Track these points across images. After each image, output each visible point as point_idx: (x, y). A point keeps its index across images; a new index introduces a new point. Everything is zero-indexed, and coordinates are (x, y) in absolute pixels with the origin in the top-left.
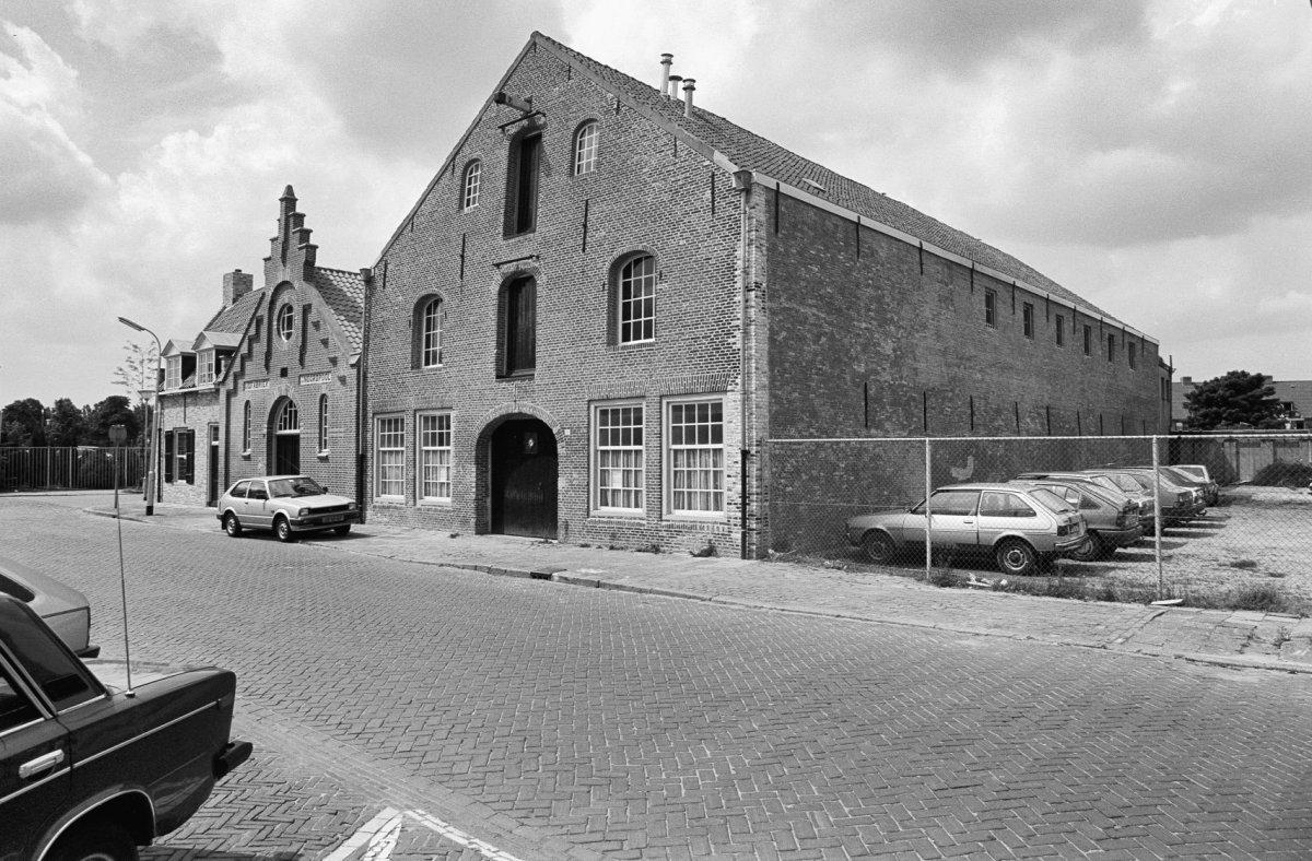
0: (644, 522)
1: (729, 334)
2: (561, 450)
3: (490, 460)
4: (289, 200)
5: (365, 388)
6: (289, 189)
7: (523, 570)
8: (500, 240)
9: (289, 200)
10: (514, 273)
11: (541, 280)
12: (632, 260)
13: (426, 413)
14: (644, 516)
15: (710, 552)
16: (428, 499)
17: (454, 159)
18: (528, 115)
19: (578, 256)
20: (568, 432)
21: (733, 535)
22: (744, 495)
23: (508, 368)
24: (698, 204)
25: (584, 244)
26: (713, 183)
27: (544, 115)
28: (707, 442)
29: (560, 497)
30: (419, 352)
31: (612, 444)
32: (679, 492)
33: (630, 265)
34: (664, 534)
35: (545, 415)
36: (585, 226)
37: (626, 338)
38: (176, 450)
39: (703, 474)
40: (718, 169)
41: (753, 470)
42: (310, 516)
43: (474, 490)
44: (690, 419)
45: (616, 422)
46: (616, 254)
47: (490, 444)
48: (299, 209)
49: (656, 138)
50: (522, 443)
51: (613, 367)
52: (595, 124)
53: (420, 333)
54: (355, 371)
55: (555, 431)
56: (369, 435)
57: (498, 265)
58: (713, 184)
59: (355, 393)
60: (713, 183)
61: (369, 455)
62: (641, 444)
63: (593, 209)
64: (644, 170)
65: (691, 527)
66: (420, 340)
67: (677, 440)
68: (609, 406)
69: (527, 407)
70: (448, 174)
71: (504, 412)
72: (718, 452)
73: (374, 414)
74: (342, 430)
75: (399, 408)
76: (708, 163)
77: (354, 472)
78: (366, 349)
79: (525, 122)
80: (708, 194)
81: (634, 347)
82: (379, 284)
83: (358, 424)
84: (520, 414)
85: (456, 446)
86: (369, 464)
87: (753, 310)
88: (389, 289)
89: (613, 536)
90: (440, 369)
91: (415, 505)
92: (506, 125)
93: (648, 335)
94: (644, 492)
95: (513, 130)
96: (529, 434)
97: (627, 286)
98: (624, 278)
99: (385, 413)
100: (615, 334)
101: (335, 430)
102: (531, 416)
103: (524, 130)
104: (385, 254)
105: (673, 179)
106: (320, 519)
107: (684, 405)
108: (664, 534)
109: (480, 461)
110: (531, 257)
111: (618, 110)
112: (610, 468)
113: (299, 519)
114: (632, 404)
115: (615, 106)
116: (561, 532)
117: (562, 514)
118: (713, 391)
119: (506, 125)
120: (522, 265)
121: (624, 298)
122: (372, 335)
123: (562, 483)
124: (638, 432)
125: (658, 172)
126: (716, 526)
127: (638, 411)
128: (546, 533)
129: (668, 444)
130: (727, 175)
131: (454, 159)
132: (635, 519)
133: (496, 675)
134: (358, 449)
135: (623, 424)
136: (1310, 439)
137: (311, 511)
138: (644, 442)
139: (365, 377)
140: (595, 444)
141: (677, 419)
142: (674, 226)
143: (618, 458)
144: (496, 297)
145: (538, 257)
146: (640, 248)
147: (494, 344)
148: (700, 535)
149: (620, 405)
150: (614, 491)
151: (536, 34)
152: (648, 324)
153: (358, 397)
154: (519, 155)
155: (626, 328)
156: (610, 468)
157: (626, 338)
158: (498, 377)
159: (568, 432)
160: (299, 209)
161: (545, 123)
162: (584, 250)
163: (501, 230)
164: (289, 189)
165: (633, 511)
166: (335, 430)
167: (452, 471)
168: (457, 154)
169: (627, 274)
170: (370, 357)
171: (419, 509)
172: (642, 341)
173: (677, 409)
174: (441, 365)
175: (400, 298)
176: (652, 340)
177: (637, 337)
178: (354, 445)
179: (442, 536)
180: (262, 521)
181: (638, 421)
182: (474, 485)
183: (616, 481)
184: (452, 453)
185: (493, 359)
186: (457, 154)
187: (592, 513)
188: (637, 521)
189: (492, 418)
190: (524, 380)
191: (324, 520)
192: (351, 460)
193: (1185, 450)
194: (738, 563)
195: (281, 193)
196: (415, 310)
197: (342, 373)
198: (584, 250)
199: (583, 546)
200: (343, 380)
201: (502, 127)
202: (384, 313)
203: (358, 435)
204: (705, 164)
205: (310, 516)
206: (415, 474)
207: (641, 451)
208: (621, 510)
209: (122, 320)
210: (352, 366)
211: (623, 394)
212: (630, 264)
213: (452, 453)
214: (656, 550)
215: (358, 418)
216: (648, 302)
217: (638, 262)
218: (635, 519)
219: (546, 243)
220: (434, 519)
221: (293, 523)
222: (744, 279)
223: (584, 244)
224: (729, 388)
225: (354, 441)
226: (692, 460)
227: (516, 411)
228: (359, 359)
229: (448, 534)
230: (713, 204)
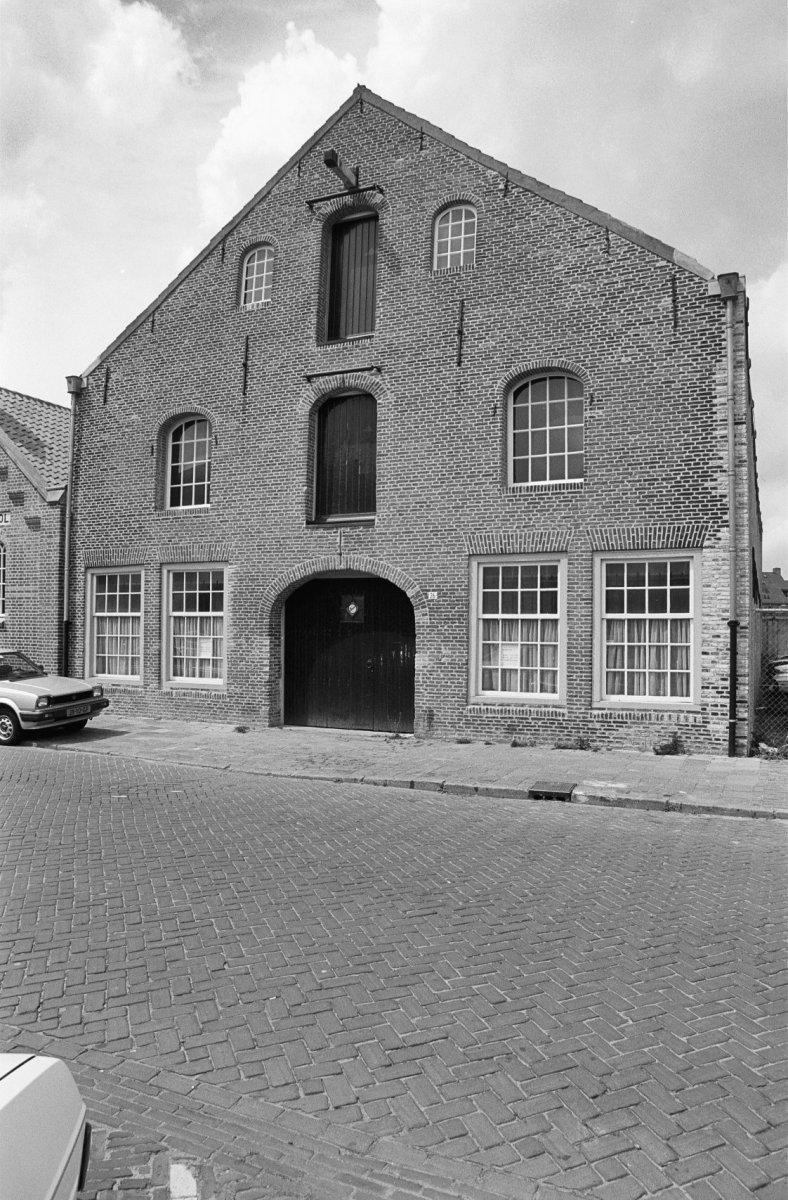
0: (565, 711)
1: (705, 476)
2: (421, 618)
3: (283, 631)
5: (73, 533)
7: (520, 788)
8: (312, 346)
10: (338, 389)
11: (385, 403)
12: (183, 423)
13: (100, 572)
15: (674, 748)
16: (178, 679)
17: (223, 241)
18: (353, 190)
19: (450, 371)
20: (433, 595)
21: (710, 727)
22: (734, 675)
23: (317, 513)
24: (650, 315)
25: (460, 355)
26: (674, 288)
27: (381, 191)
29: (419, 678)
30: (163, 489)
32: (112, 657)
33: (178, 426)
34: (598, 726)
35: (395, 574)
36: (460, 333)
37: (175, 502)
39: (654, 651)
40: (682, 270)
41: (744, 645)
42: (51, 708)
43: (267, 669)
44: (191, 586)
45: (191, 586)
46: (514, 371)
47: (283, 611)
49: (575, 229)
50: (338, 610)
51: (512, 513)
52: (266, 248)
53: (164, 464)
54: (57, 511)
55: (410, 593)
56: (78, 596)
57: (309, 379)
58: (674, 291)
59: (57, 540)
60: (674, 288)
61: (78, 622)
62: (556, 612)
63: (470, 314)
64: (556, 268)
65: (642, 717)
66: (164, 472)
67: (100, 607)
68: (500, 563)
69: (361, 562)
70: (213, 260)
71: (319, 568)
72: (681, 625)
73: (87, 568)
74: (31, 588)
75: (132, 560)
76: (664, 263)
77: (55, 644)
78: (75, 482)
79: (348, 199)
80: (667, 301)
81: (548, 487)
82: (96, 398)
83: (61, 581)
84: (349, 570)
85: (235, 611)
86: (79, 633)
88: (113, 404)
89: (511, 729)
90: (206, 511)
91: (159, 688)
92: (316, 201)
93: (200, 501)
94: (142, 659)
95: (328, 208)
96: (350, 596)
97: (176, 449)
98: (174, 441)
99: (107, 567)
100: (163, 498)
101: (17, 588)
102: (368, 573)
103: (346, 209)
104: (105, 357)
105: (606, 281)
106: (64, 711)
107: (539, 565)
108: (598, 726)
109: (273, 633)
110: (371, 369)
111: (506, 189)
112: (500, 642)
113: (38, 712)
114: (539, 561)
115: (501, 186)
116: (420, 725)
117: (422, 700)
118: (680, 546)
119: (316, 201)
120: (351, 380)
121: (173, 462)
122: (83, 464)
123: (421, 661)
124: (136, 600)
125: (575, 270)
126: (682, 715)
127: (137, 578)
128: (396, 725)
129: (168, 611)
130: (697, 280)
131: (223, 241)
132: (546, 706)
133: (41, 863)
134: (61, 614)
137: (52, 700)
139: (73, 519)
140: (91, 609)
141: (178, 585)
142: (612, 339)
143: (489, 625)
144: (305, 419)
145: (379, 370)
146: (555, 364)
147: (303, 479)
148: (658, 728)
149: (520, 562)
150: (202, 660)
151: (361, 90)
152: (200, 489)
153: (62, 545)
154: (330, 242)
155: (175, 493)
156: (500, 642)
157: (175, 502)
158: (308, 523)
159: (433, 595)
161: (383, 203)
162: (459, 363)
163: (312, 333)
165: (548, 696)
166: (17, 588)
167: (227, 645)
168: (230, 233)
169: (177, 436)
170: (80, 493)
171: (167, 694)
172: (193, 506)
173: (178, 577)
174: (209, 506)
175: (134, 417)
176: (206, 505)
177: (187, 502)
178: (54, 610)
179: (221, 731)
181: (137, 588)
182: (266, 662)
183: (510, 657)
184: (227, 622)
185: (301, 499)
186: (230, 233)
187: (472, 700)
188: (551, 709)
189: (299, 576)
190: (358, 526)
191: (68, 714)
192: (52, 626)
194: (722, 762)
196: (160, 430)
197: (32, 513)
198: (459, 363)
199: (461, 742)
200: (34, 524)
201: (311, 204)
202: (105, 437)
203: (61, 595)
204: (658, 265)
205: (51, 708)
206: (160, 647)
207: (139, 618)
208: (516, 695)
210: (52, 504)
211: (530, 547)
212: (181, 426)
213: (227, 622)
214: (583, 745)
215: (61, 573)
216: (200, 468)
217: (189, 425)
218: (546, 706)
219: (392, 351)
220: (208, 707)
221: (26, 718)
222: (733, 409)
223: (460, 355)
224: (706, 543)
225: (54, 601)
227: (342, 567)
228: (64, 496)
229: (233, 727)
230: (676, 315)
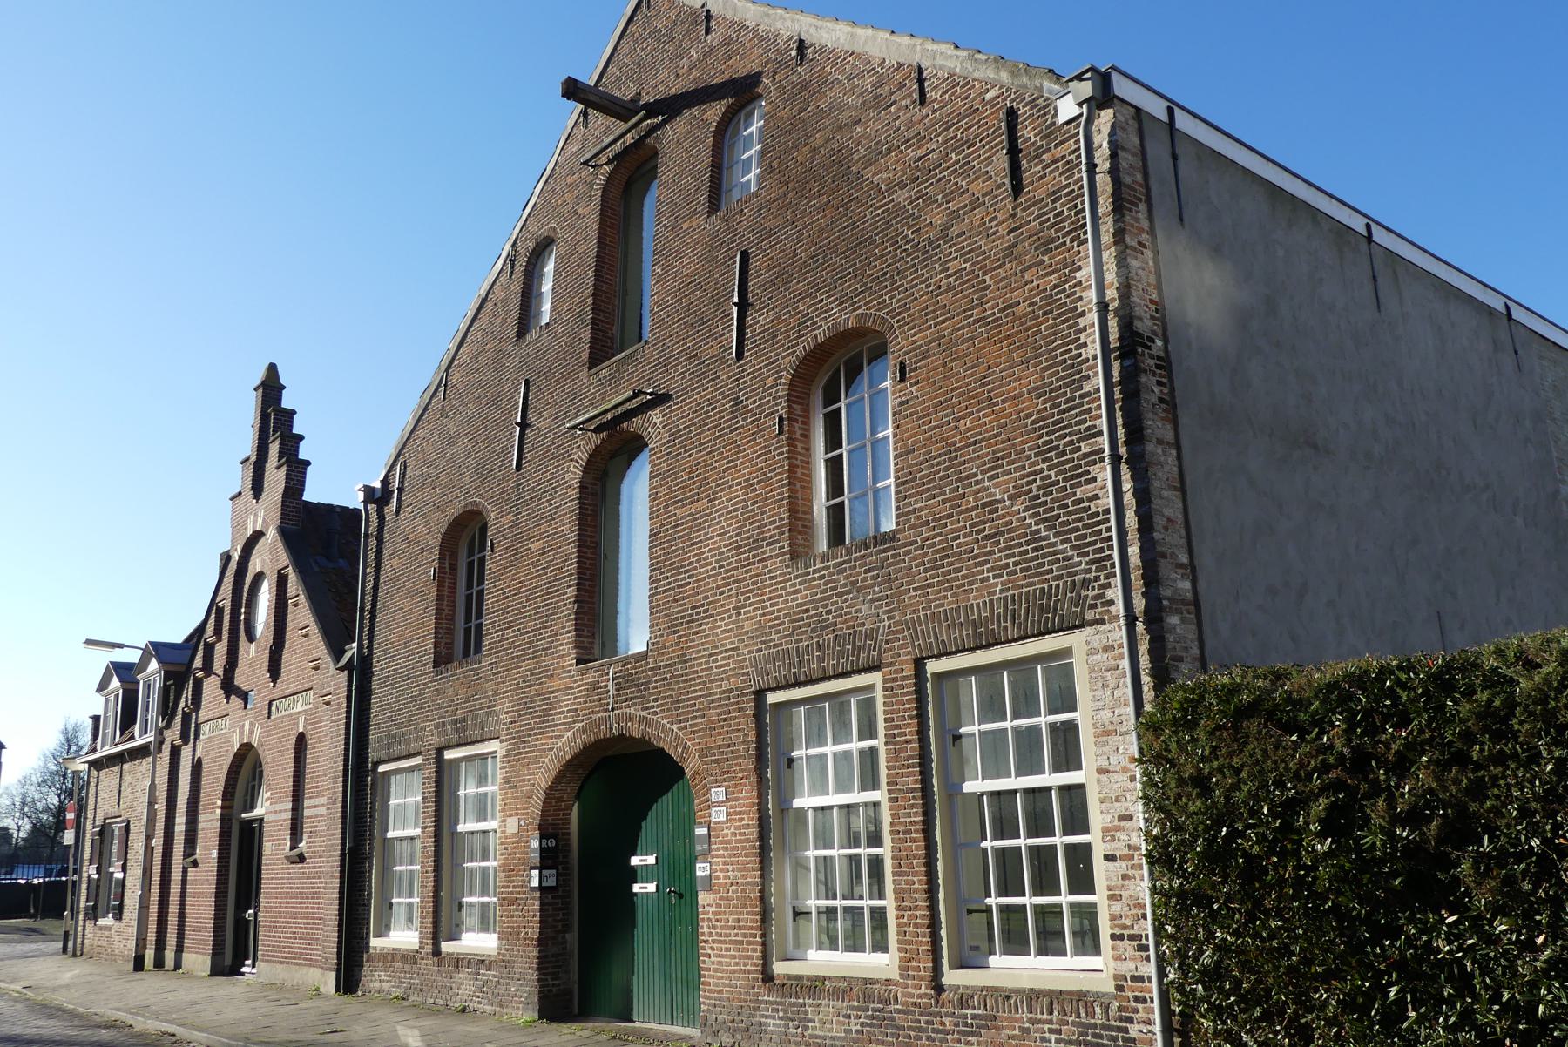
4: (271, 388)
6: (272, 369)
9: (271, 388)
14: (895, 974)
28: (1039, 770)
29: (705, 928)
31: (1057, 769)
38: (257, 829)
48: (286, 403)
87: (1154, 352)
135: (1035, 730)
136: (2, 960)
138: (883, 780)
160: (286, 403)
164: (272, 369)
180: (411, 942)
193: (390, 958)
195: (258, 376)
200: (1119, 627)
207: (1082, 787)
209: (89, 642)
224: (1089, 615)
226: (671, 849)
